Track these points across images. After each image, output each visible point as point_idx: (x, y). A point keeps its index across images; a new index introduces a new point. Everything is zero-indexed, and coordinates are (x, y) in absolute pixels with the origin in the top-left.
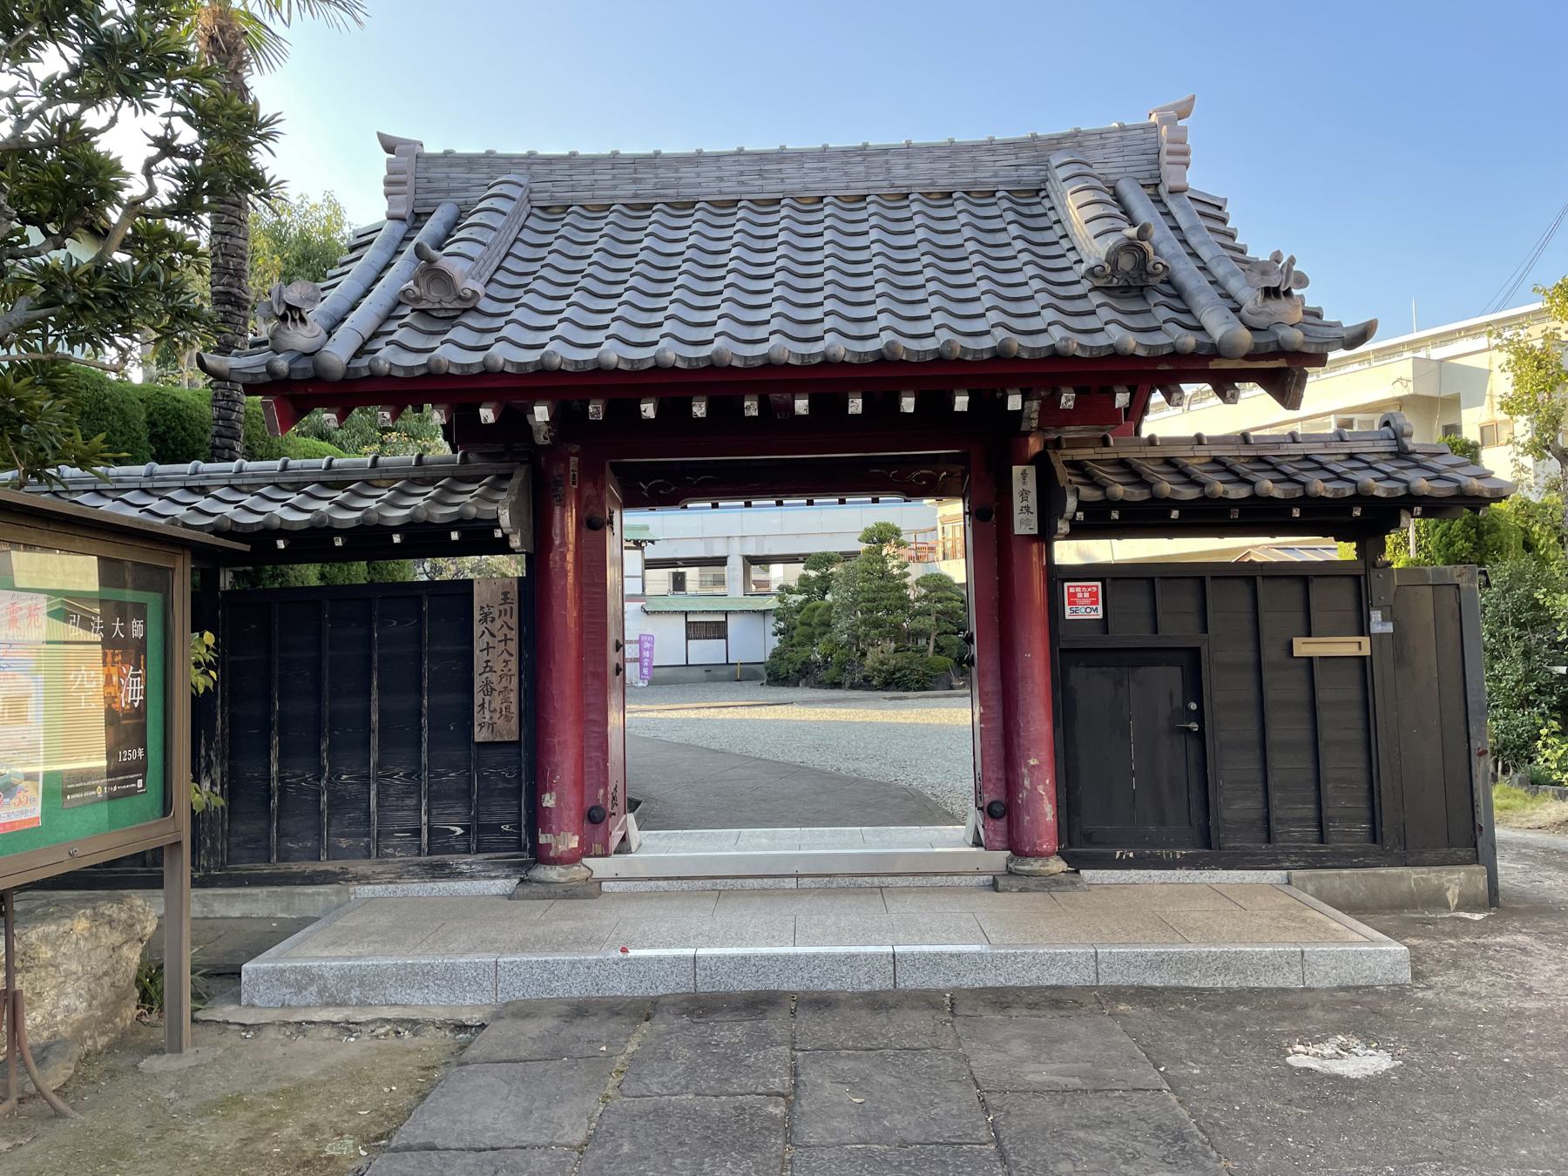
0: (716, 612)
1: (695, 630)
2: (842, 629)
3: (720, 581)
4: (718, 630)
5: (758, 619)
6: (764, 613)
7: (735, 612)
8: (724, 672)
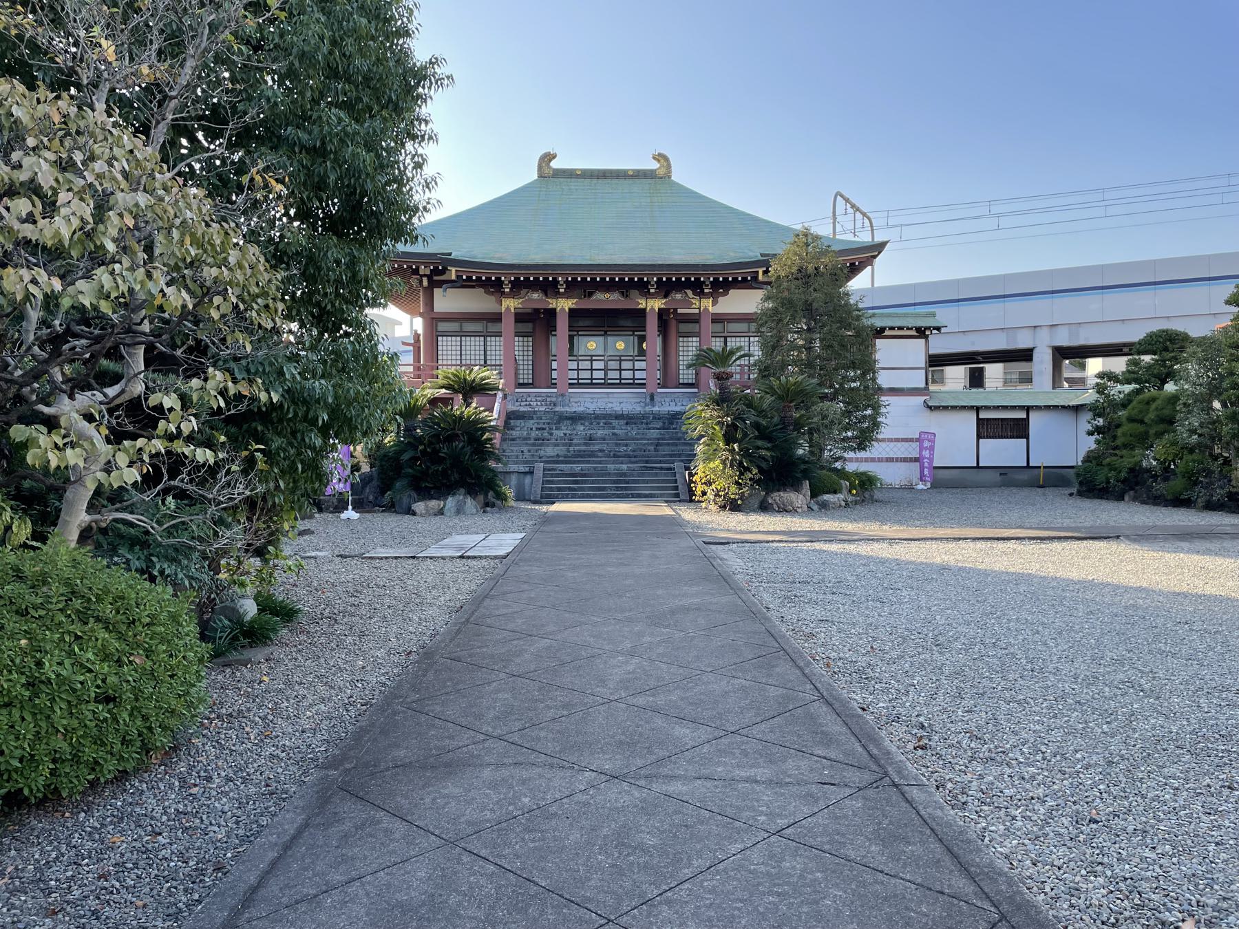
0: (1013, 408)
1: (987, 429)
2: (1188, 427)
3: (1027, 379)
4: (1018, 429)
5: (1068, 418)
6: (1077, 409)
7: (1038, 408)
8: (1024, 476)
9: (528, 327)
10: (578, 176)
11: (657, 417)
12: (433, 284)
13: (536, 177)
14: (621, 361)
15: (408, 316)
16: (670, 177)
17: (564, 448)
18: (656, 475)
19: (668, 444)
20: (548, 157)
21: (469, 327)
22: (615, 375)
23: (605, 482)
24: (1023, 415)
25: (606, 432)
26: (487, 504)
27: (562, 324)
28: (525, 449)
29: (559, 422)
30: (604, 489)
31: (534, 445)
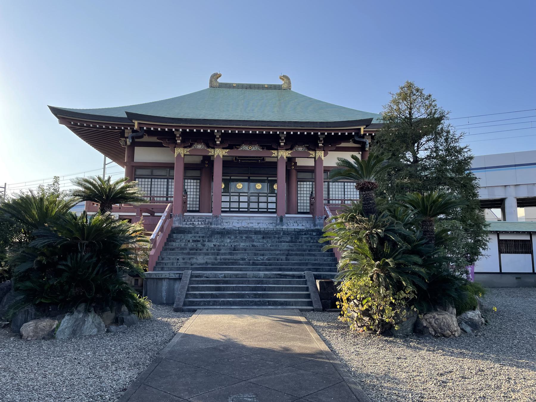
9: (197, 173)
10: (234, 87)
11: (286, 233)
12: (134, 144)
13: (208, 86)
14: (259, 196)
15: (102, 156)
16: (290, 89)
17: (212, 257)
18: (290, 283)
19: (296, 255)
20: (216, 76)
21: (157, 172)
22: (255, 205)
23: (243, 289)
24: (528, 238)
25: (248, 244)
26: (118, 321)
27: (218, 169)
28: (180, 257)
29: (211, 236)
30: (242, 296)
31: (189, 254)
